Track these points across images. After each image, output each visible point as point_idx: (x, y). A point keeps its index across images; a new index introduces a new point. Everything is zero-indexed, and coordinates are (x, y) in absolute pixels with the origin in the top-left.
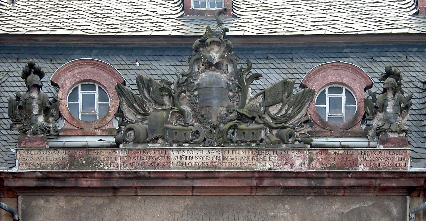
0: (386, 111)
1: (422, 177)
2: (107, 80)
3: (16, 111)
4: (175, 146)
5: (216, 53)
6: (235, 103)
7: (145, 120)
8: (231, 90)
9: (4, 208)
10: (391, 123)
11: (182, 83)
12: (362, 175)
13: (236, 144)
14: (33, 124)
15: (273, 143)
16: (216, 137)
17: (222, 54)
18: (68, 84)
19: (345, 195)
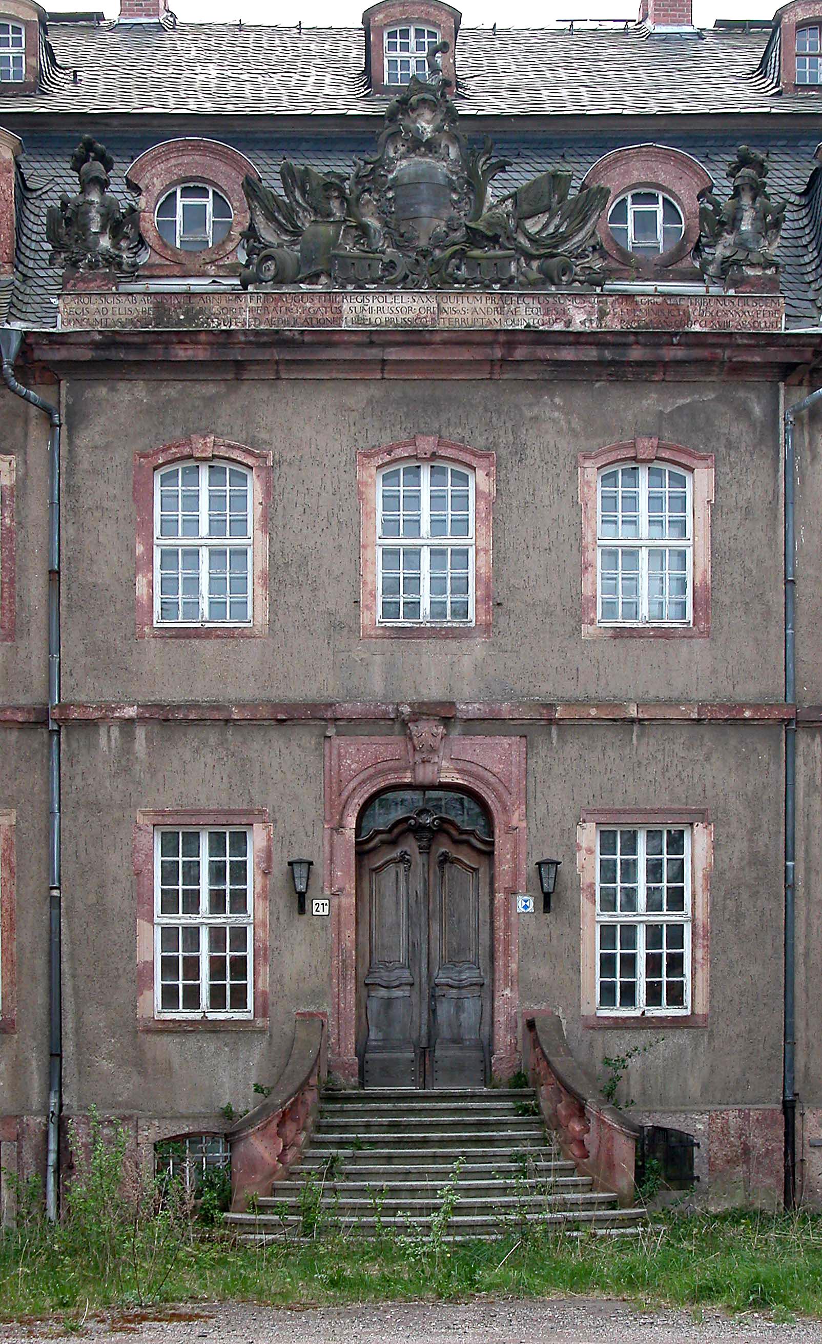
0: (739, 228)
1: (809, 345)
2: (228, 177)
3: (60, 230)
4: (350, 288)
5: (428, 123)
6: (462, 213)
7: (295, 245)
8: (454, 190)
9: (32, 400)
10: (749, 251)
11: (365, 176)
13: (464, 286)
14: (89, 250)
15: (533, 284)
16: (426, 272)
17: (438, 126)
18: (158, 184)
19: (667, 379)
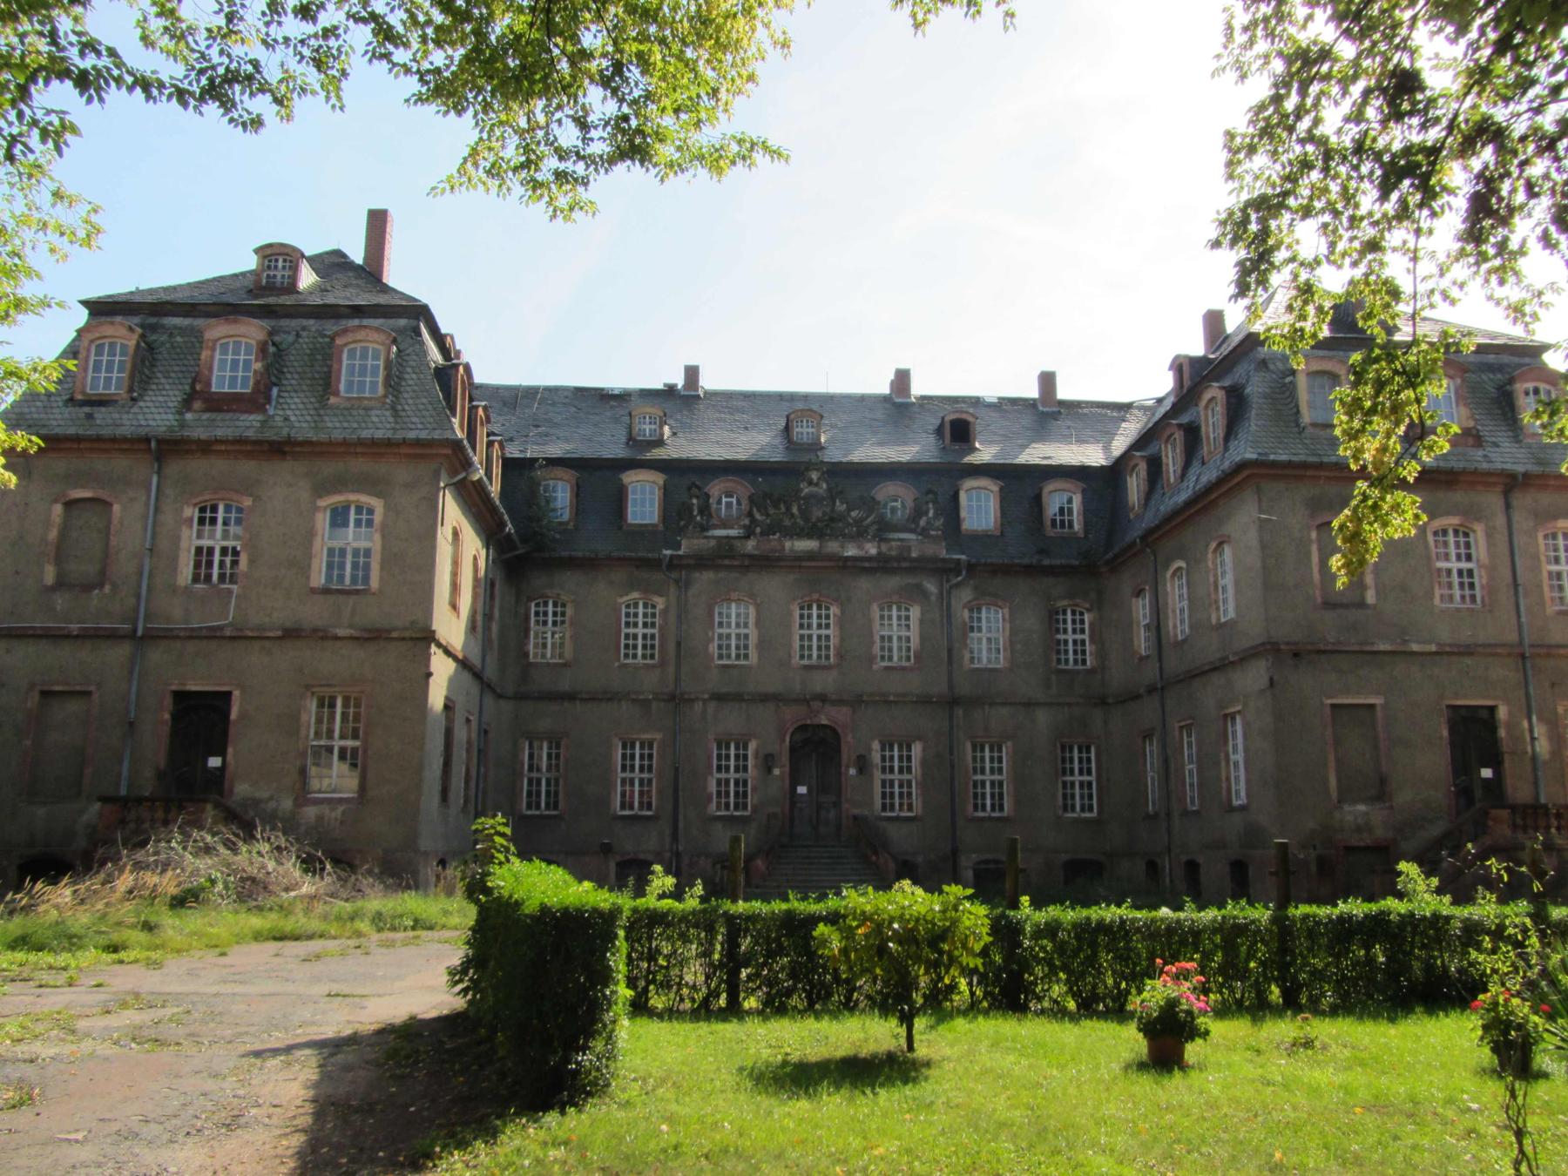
12: (915, 560)
18: (716, 494)
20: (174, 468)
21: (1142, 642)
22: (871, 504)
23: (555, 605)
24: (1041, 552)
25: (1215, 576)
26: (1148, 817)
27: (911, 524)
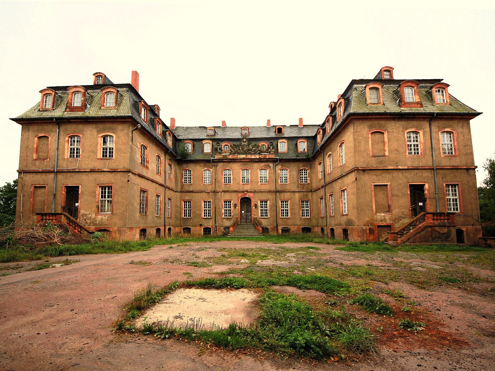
20: (63, 128)
21: (320, 176)
22: (257, 146)
23: (189, 171)
24: (297, 156)
25: (340, 153)
26: (321, 217)
27: (267, 151)
